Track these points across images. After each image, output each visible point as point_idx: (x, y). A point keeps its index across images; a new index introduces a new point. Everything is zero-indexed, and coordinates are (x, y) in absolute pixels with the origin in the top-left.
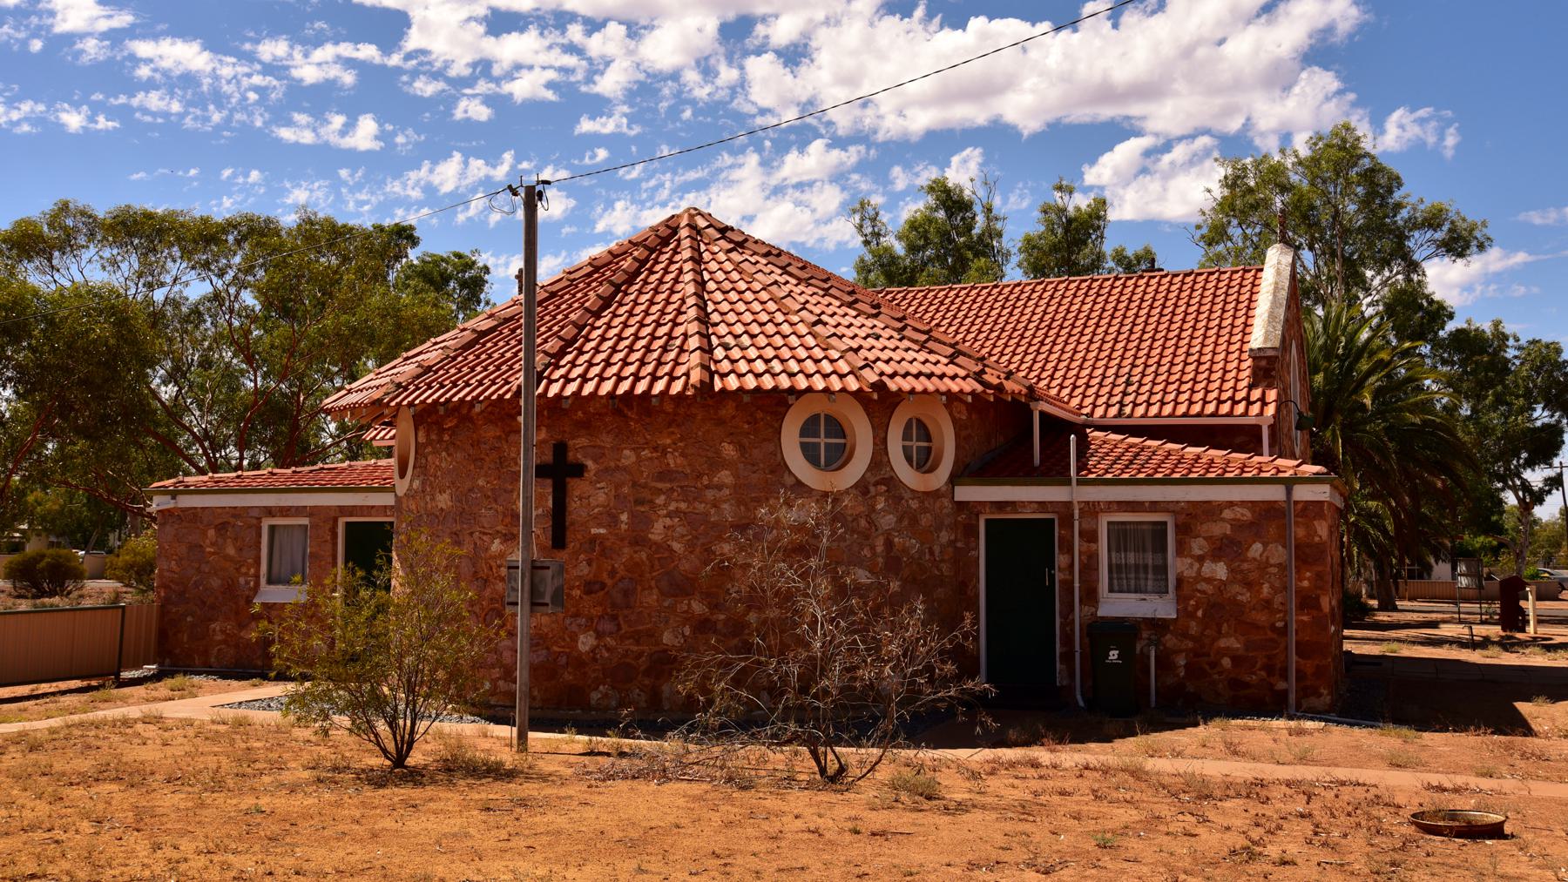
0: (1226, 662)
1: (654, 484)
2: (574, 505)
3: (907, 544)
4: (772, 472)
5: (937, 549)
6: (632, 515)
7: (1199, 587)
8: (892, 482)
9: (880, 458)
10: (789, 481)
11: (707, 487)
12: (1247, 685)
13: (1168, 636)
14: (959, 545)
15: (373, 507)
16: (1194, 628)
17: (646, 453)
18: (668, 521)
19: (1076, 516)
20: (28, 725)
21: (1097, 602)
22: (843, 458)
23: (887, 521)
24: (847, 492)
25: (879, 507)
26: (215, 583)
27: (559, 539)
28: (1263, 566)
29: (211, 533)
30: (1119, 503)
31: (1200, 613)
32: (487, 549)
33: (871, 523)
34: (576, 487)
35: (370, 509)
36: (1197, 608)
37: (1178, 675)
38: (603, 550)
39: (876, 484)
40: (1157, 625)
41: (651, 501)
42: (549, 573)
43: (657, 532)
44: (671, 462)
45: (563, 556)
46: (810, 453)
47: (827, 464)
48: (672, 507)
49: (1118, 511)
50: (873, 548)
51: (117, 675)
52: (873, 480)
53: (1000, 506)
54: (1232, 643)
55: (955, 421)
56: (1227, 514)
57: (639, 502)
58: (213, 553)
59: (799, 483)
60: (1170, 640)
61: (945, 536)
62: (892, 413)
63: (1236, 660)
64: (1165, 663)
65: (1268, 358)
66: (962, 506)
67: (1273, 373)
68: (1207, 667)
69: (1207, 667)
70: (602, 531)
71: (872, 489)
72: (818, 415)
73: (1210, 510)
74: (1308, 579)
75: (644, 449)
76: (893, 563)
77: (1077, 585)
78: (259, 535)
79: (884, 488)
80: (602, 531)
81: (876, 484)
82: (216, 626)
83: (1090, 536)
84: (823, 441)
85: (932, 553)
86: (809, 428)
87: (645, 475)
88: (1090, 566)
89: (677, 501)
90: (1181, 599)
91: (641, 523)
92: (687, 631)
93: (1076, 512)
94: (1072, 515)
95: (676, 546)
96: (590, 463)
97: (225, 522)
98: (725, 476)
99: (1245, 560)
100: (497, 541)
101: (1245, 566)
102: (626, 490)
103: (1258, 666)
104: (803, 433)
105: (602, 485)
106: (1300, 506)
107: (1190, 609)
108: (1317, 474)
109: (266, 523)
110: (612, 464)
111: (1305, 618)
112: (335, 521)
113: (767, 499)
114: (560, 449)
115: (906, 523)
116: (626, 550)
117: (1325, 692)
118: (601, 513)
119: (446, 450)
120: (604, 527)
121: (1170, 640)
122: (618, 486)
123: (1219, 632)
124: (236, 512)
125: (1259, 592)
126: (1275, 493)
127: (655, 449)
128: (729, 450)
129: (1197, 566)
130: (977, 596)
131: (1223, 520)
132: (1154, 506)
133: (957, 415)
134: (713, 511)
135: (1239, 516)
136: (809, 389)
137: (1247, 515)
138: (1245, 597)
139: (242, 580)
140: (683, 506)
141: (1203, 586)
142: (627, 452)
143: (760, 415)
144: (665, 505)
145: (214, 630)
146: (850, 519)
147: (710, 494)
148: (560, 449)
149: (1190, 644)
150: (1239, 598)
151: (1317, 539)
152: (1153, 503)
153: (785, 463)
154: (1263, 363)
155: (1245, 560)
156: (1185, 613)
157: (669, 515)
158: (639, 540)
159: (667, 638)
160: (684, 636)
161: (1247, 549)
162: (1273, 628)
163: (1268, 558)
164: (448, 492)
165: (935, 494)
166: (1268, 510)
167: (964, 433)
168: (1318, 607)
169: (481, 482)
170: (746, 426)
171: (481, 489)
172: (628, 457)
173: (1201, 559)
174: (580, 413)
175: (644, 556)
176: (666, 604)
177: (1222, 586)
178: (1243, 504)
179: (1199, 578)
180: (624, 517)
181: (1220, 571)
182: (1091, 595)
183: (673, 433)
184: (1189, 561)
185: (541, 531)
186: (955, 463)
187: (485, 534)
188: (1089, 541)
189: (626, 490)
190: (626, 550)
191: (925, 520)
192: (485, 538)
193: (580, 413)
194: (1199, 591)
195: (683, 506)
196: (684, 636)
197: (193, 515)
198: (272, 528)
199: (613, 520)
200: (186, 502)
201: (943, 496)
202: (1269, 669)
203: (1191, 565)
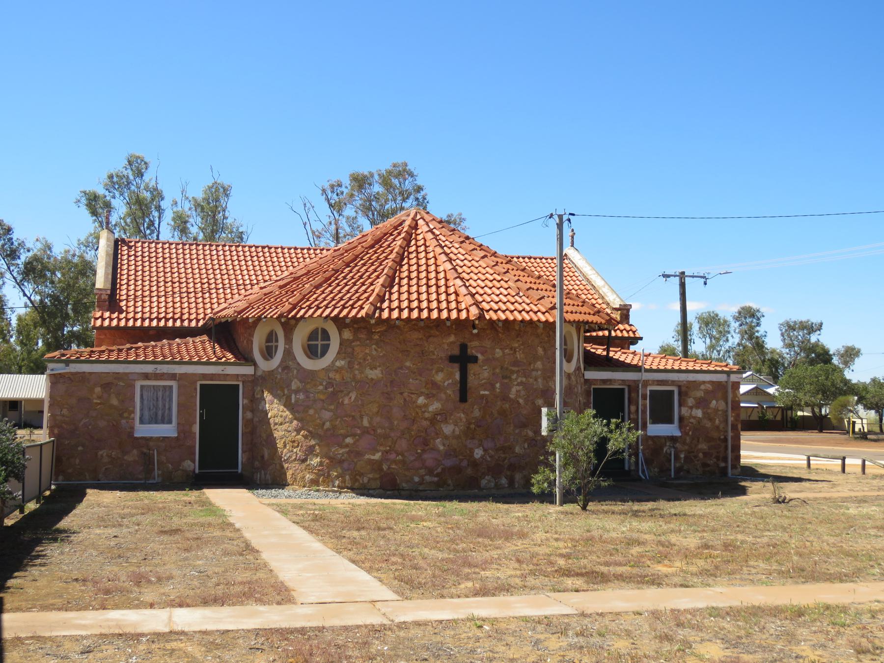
0: (701, 455)
1: (510, 368)
2: (471, 379)
6: (502, 384)
11: (533, 370)
12: (708, 465)
15: (228, 375)
16: (688, 440)
17: (507, 351)
18: (518, 388)
22: (309, 353)
26: (102, 424)
27: (463, 398)
28: (716, 410)
29: (98, 390)
30: (658, 381)
31: (690, 433)
34: (472, 368)
35: (226, 376)
38: (487, 402)
40: (673, 439)
41: (510, 378)
44: (518, 356)
45: (466, 406)
48: (519, 380)
54: (703, 446)
56: (703, 387)
57: (504, 377)
63: (705, 454)
70: (487, 393)
73: (696, 385)
80: (487, 393)
82: (102, 453)
91: (506, 388)
92: (526, 446)
94: (638, 387)
95: (521, 401)
96: (480, 356)
97: (109, 383)
98: (539, 365)
99: (709, 408)
102: (498, 371)
103: (714, 456)
105: (486, 367)
109: (138, 384)
110: (491, 357)
112: (195, 382)
114: (464, 347)
116: (499, 403)
119: (377, 344)
120: (488, 391)
121: (678, 445)
122: (494, 369)
123: (698, 442)
124: (118, 376)
125: (714, 422)
127: (511, 349)
129: (690, 411)
131: (701, 390)
137: (709, 387)
138: (708, 424)
139: (124, 421)
140: (524, 379)
141: (692, 420)
142: (498, 350)
144: (516, 379)
145: (102, 456)
147: (534, 373)
148: (464, 347)
149: (686, 447)
155: (709, 408)
158: (505, 398)
160: (525, 449)
162: (719, 439)
164: (379, 369)
169: (408, 364)
171: (408, 368)
172: (498, 353)
173: (691, 408)
175: (507, 406)
177: (699, 421)
179: (691, 416)
180: (498, 385)
181: (699, 413)
184: (686, 408)
185: (453, 393)
187: (412, 393)
189: (498, 371)
190: (499, 403)
192: (413, 396)
194: (691, 423)
196: (525, 449)
197: (83, 377)
198: (142, 387)
200: (74, 368)
202: (718, 458)
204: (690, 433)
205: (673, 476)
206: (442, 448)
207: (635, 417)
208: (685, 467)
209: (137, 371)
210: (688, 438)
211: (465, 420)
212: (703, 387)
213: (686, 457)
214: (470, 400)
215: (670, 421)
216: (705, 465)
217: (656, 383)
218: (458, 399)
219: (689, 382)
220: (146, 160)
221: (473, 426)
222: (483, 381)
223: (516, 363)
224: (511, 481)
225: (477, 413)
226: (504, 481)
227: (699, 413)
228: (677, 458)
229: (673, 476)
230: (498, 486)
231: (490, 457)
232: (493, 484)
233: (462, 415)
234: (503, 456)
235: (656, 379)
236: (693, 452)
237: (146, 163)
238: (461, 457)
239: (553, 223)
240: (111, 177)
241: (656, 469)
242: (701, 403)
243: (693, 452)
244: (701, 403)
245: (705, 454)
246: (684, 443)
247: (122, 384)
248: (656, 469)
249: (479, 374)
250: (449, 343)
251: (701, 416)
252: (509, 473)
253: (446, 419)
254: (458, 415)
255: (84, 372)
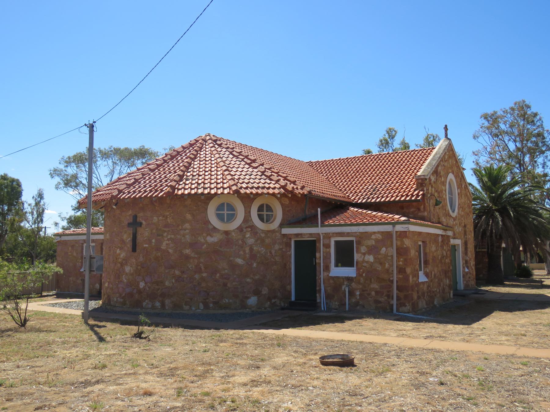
0: (373, 293)
2: (139, 237)
3: (260, 250)
4: (204, 224)
5: (273, 252)
7: (364, 265)
8: (253, 227)
9: (247, 218)
10: (210, 227)
11: (181, 230)
12: (380, 302)
13: (353, 283)
14: (284, 250)
16: (362, 280)
17: (161, 218)
18: (167, 242)
19: (322, 239)
20: (415, 316)
21: (330, 271)
23: (251, 241)
24: (234, 231)
25: (247, 236)
27: (134, 249)
28: (386, 256)
29: (70, 248)
30: (336, 233)
31: (364, 275)
32: (116, 252)
33: (244, 242)
34: (140, 230)
36: (363, 272)
37: (357, 298)
39: (246, 228)
41: (162, 235)
42: (95, 260)
43: (164, 247)
45: (136, 254)
46: (261, 217)
47: (267, 221)
48: (169, 237)
49: (336, 236)
50: (244, 251)
51: (41, 294)
52: (245, 226)
53: (297, 235)
54: (375, 286)
55: (282, 205)
57: (158, 235)
58: (71, 255)
59: (214, 228)
60: (354, 285)
61: (277, 247)
62: (253, 202)
63: (377, 293)
64: (351, 293)
65: (422, 179)
66: (284, 235)
67: (424, 185)
68: (366, 295)
69: (366, 295)
70: (147, 246)
71: (245, 230)
72: (224, 203)
74: (402, 261)
75: (160, 217)
76: (253, 256)
77: (322, 264)
78: (83, 249)
79: (250, 229)
80: (147, 246)
81: (246, 228)
82: (71, 279)
83: (328, 246)
84: (265, 213)
85: (271, 253)
86: (260, 209)
87: (160, 225)
88: (327, 257)
89: (171, 235)
90: (358, 269)
92: (174, 281)
93: (322, 237)
95: (170, 251)
96: (144, 222)
98: (187, 226)
100: (118, 250)
101: (380, 257)
102: (154, 231)
103: (384, 295)
104: (259, 211)
105: (147, 229)
106: (398, 233)
107: (360, 273)
108: (404, 220)
111: (401, 276)
113: (202, 234)
114: (135, 217)
115: (259, 242)
117: (408, 305)
118: (146, 240)
121: (354, 285)
123: (371, 282)
126: (389, 228)
127: (164, 216)
128: (189, 216)
129: (363, 257)
130: (290, 269)
131: (372, 239)
132: (348, 234)
133: (284, 202)
134: (183, 238)
135: (377, 237)
136: (216, 194)
137: (379, 236)
138: (379, 268)
140: (173, 236)
141: (365, 264)
142: (155, 218)
143: (200, 203)
144: (167, 236)
146: (235, 240)
147: (182, 232)
148: (135, 217)
149: (361, 287)
150: (378, 269)
151: (405, 246)
152: (348, 233)
153: (209, 221)
154: (420, 181)
156: (359, 274)
157: (168, 240)
158: (158, 249)
159: (167, 283)
160: (172, 283)
161: (380, 250)
163: (387, 253)
165: (273, 231)
166: (388, 235)
167: (287, 209)
168: (405, 272)
170: (195, 208)
172: (155, 219)
173: (364, 254)
174: (141, 205)
175: (159, 254)
176: (167, 271)
177: (371, 264)
178: (379, 232)
179: (364, 261)
180: (154, 241)
181: (371, 258)
182: (327, 268)
183: (170, 211)
185: (129, 245)
186: (282, 220)
188: (326, 248)
189: (154, 231)
191: (267, 241)
193: (141, 205)
194: (364, 266)
195: (173, 236)
196: (172, 283)
199: (150, 242)
201: (277, 232)
203: (361, 257)
204: (364, 275)
205: (347, 309)
206: (125, 281)
207: (319, 262)
208: (361, 302)
209: (81, 239)
210: (362, 279)
211: (135, 263)
212: (373, 237)
213: (360, 295)
214: (138, 251)
215: (351, 264)
216: (377, 302)
217: (335, 235)
218: (131, 250)
219: (362, 233)
220: (395, 129)
221: (139, 267)
222: (145, 238)
223: (166, 226)
224: (163, 305)
225: (141, 259)
226: (158, 304)
227: (371, 258)
228: (351, 293)
229: (347, 309)
230: (153, 307)
231: (148, 287)
232: (150, 306)
233: (134, 261)
234: (157, 287)
235: (334, 232)
236: (367, 290)
237: (395, 131)
238: (133, 287)
239: (86, 130)
240: (381, 141)
241: (336, 303)
242: (372, 250)
243: (367, 290)
244: (372, 250)
245: (377, 293)
246: (359, 283)
247: (77, 245)
248: (336, 303)
249: (144, 233)
250: (127, 216)
251: (372, 261)
252: (160, 299)
253: (127, 262)
254: (132, 260)
255: (65, 240)
